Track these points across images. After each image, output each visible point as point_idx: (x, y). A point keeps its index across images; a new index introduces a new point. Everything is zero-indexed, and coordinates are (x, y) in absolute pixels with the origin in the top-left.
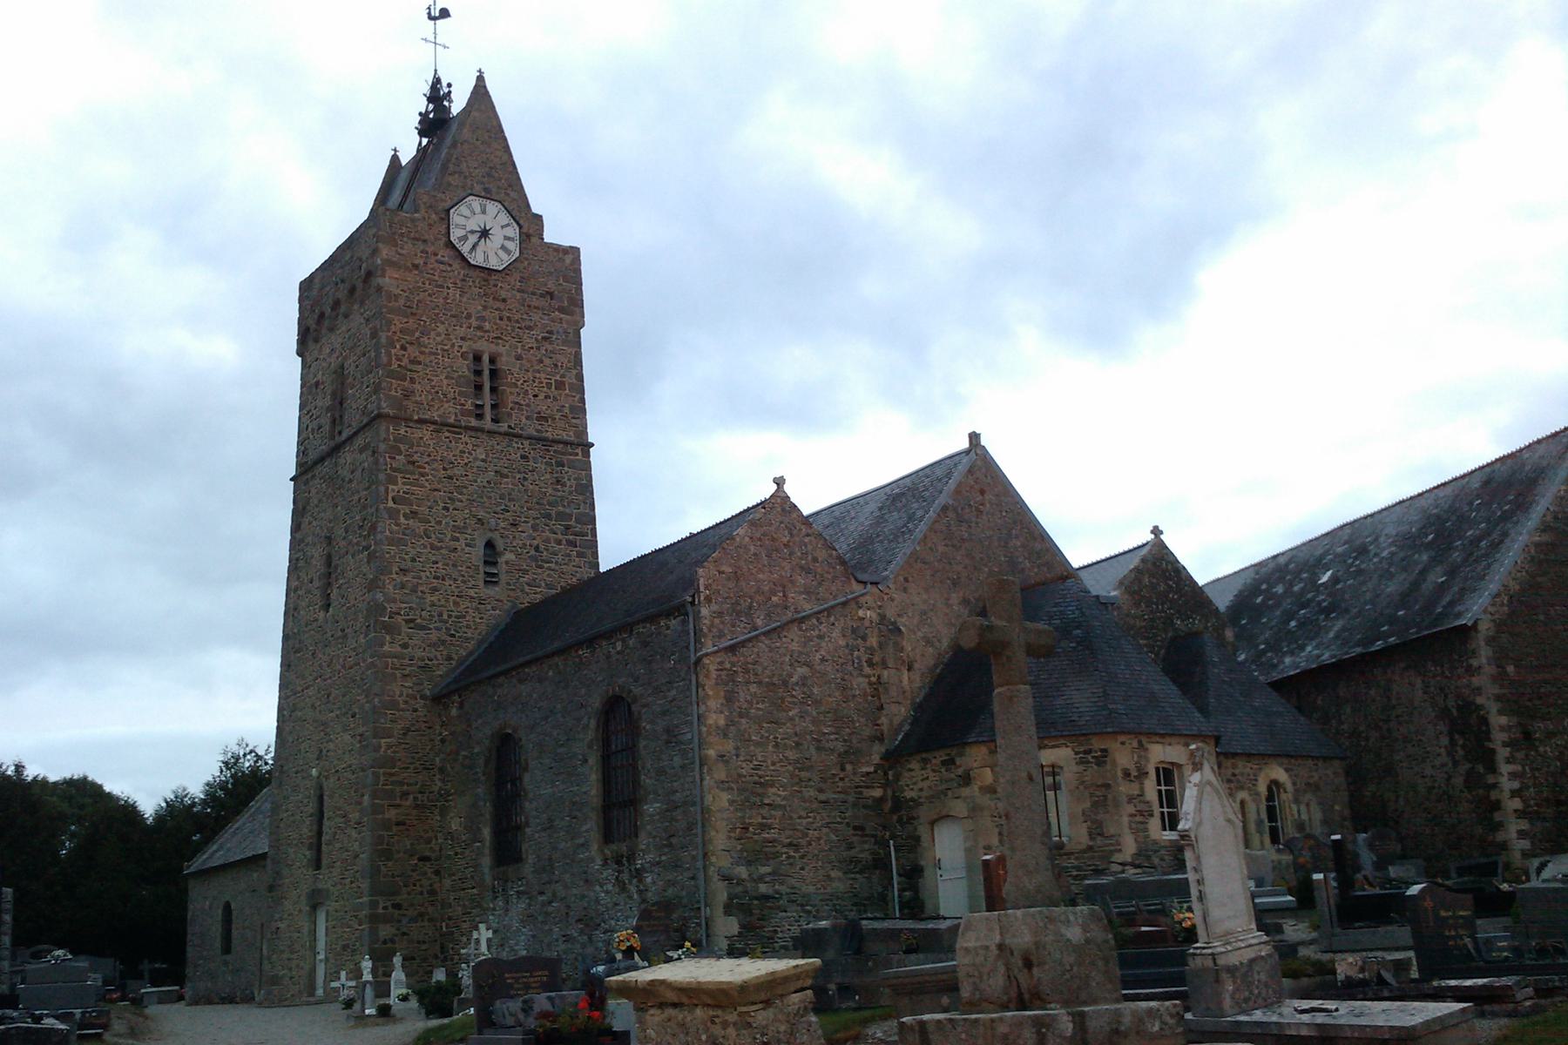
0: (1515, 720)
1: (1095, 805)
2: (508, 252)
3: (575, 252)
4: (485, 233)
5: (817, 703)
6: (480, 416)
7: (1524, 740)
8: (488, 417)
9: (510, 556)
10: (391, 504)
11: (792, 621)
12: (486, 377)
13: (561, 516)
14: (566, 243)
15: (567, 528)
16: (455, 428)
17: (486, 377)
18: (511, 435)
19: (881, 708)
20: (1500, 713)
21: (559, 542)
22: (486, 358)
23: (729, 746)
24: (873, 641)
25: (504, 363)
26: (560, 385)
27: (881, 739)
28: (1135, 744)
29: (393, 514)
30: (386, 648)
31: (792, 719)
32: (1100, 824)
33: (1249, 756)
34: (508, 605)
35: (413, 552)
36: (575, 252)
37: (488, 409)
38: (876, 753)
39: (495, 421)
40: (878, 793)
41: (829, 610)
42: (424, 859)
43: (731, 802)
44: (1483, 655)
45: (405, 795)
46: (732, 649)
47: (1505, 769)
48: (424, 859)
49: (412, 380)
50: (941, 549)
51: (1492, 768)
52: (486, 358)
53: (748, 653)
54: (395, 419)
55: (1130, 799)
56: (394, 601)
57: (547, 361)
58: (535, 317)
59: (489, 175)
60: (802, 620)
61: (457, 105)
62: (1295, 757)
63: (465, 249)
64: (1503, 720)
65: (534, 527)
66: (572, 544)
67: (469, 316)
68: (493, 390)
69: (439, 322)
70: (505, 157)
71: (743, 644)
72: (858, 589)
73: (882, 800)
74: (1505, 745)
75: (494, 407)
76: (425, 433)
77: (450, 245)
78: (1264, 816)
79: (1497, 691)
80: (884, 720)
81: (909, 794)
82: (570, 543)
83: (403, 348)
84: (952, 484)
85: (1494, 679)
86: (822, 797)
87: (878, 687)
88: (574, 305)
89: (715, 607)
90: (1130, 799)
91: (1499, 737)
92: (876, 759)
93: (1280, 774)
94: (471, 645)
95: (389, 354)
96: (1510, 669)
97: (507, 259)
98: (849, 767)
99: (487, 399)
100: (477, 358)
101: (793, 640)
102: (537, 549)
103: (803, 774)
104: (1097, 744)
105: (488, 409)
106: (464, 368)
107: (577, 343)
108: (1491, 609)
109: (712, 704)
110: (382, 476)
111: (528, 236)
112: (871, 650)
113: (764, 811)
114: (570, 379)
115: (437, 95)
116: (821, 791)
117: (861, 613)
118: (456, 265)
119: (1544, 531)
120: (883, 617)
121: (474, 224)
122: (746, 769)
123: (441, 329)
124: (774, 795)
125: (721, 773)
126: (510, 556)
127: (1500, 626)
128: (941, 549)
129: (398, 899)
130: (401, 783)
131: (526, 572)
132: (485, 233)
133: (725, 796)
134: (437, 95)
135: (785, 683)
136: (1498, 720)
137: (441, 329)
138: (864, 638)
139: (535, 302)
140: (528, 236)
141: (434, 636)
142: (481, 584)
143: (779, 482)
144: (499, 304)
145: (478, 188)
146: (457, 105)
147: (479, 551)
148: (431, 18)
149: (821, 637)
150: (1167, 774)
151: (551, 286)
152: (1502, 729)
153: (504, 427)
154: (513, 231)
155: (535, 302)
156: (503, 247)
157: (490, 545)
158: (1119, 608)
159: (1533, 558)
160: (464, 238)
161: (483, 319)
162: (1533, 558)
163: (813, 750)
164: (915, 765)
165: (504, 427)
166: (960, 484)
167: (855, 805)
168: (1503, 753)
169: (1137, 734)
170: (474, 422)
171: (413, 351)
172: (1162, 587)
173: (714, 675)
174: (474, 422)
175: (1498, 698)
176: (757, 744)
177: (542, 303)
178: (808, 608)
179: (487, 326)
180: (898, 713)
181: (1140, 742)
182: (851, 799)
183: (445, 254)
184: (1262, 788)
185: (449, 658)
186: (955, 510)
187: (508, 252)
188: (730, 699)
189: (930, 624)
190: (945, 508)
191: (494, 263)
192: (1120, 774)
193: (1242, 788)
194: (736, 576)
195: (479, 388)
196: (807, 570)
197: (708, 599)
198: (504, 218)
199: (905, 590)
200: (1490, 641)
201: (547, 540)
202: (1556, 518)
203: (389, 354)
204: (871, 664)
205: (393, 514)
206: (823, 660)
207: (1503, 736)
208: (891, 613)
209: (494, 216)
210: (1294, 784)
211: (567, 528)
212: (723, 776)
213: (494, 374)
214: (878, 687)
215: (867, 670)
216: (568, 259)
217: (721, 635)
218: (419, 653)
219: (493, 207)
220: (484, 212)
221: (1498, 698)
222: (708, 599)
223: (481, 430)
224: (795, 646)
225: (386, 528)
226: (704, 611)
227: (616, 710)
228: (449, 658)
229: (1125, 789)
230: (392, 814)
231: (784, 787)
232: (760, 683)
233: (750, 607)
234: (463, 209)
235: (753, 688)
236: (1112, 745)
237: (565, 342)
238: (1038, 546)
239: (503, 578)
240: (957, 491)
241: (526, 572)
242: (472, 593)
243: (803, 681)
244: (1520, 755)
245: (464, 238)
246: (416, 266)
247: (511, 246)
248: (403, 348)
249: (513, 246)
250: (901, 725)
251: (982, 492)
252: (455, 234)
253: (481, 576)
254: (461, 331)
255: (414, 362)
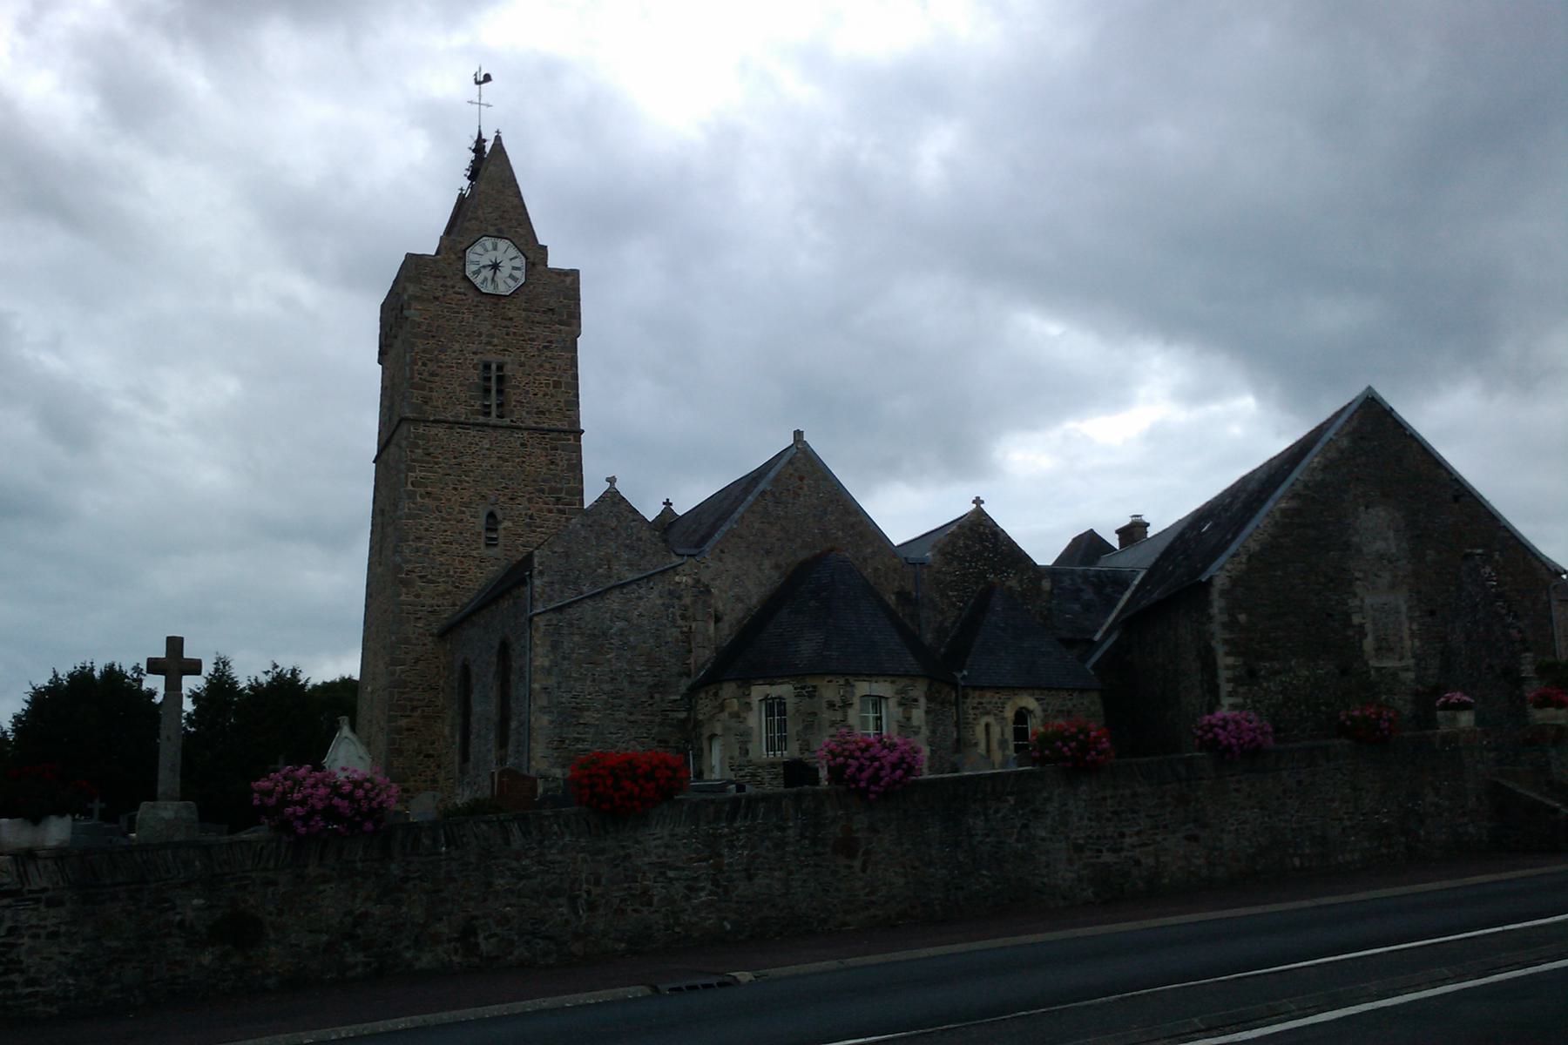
0: (1239, 661)
1: (806, 728)
2: (515, 279)
3: (575, 274)
4: (495, 266)
5: (634, 648)
6: (488, 414)
7: (1248, 677)
8: (494, 414)
9: (507, 524)
10: (410, 487)
11: (614, 587)
12: (494, 381)
13: (553, 490)
14: (567, 267)
15: (558, 499)
16: (464, 425)
17: (494, 381)
18: (512, 428)
19: (690, 651)
20: (1227, 654)
21: (550, 511)
22: (494, 367)
23: (552, 681)
24: (687, 600)
25: (508, 371)
26: (557, 385)
27: (689, 675)
28: (842, 682)
29: (411, 496)
30: (403, 598)
31: (609, 660)
32: (808, 744)
33: (997, 688)
34: (504, 563)
35: (426, 524)
36: (575, 274)
37: (494, 407)
38: (684, 685)
39: (500, 416)
40: (683, 715)
41: (648, 578)
42: (428, 756)
43: (551, 722)
44: (1217, 604)
45: (414, 709)
46: (559, 609)
47: (1226, 701)
48: (428, 756)
49: (431, 390)
50: (756, 525)
51: (1218, 703)
52: (494, 367)
53: (574, 612)
54: (415, 421)
55: (833, 724)
56: (408, 561)
57: (547, 366)
58: (538, 330)
59: (502, 217)
60: (623, 586)
61: (488, 146)
62: (1050, 689)
63: (478, 281)
64: (1230, 660)
65: (530, 500)
66: (561, 512)
67: (480, 335)
68: (500, 392)
69: (478, 325)
70: (516, 201)
71: (569, 605)
72: (676, 560)
73: (686, 720)
74: (1228, 680)
75: (500, 405)
76: (440, 431)
77: (466, 278)
78: (1009, 735)
79: (1227, 636)
80: (692, 660)
81: (700, 717)
82: (561, 512)
83: (424, 364)
84: (772, 474)
85: (1224, 626)
86: (632, 718)
87: (688, 636)
88: (571, 318)
89: (546, 579)
90: (833, 724)
91: (1223, 674)
92: (683, 689)
93: (1029, 702)
94: (471, 595)
95: (412, 370)
96: (1242, 618)
97: (513, 285)
98: (657, 696)
99: (493, 400)
100: (487, 367)
101: (615, 602)
102: (531, 517)
103: (617, 701)
104: (810, 682)
105: (494, 407)
106: (475, 376)
107: (574, 348)
108: (1228, 567)
109: (539, 650)
110: (403, 466)
111: (534, 264)
112: (686, 608)
113: (580, 728)
114: (566, 378)
115: (480, 141)
116: (631, 714)
117: (677, 579)
118: (471, 294)
119: (1292, 498)
120: (698, 581)
121: (486, 260)
122: (566, 698)
123: (457, 346)
124: (588, 717)
125: (543, 701)
126: (507, 524)
127: (1235, 582)
128: (756, 525)
129: (406, 785)
130: (411, 700)
131: (520, 536)
132: (495, 266)
133: (546, 719)
134: (480, 141)
135: (604, 634)
136: (1224, 660)
137: (457, 346)
138: (680, 598)
139: (538, 318)
140: (534, 264)
141: (442, 588)
142: (483, 546)
143: (611, 480)
144: (508, 323)
145: (491, 230)
146: (488, 146)
147: (482, 520)
148: (478, 83)
149: (640, 598)
150: (877, 701)
151: (553, 304)
152: (1228, 667)
153: (507, 421)
154: (520, 262)
155: (538, 318)
156: (511, 276)
157: (491, 515)
158: (929, 566)
159: (1276, 523)
160: (477, 272)
161: (492, 336)
162: (1276, 523)
163: (626, 684)
164: (703, 695)
165: (507, 421)
166: (779, 474)
167: (661, 724)
168: (1226, 687)
169: (844, 674)
170: (481, 419)
171: (432, 366)
172: (978, 547)
173: (542, 629)
174: (481, 419)
175: (1226, 642)
176: (576, 680)
177: (545, 318)
178: (630, 576)
179: (495, 341)
180: (703, 655)
181: (847, 682)
182: (657, 720)
183: (461, 287)
184: (1009, 713)
185: (454, 605)
186: (773, 494)
187: (515, 279)
188: (555, 647)
189: (738, 582)
190: (763, 493)
191: (503, 289)
192: (825, 705)
193: (988, 713)
194: (567, 555)
195: (487, 391)
196: (630, 548)
197: (541, 573)
198: (513, 252)
199: (720, 560)
200: (1223, 593)
201: (541, 510)
202: (1306, 486)
203: (412, 370)
204: (683, 617)
205: (411, 496)
206: (640, 615)
207: (1229, 674)
208: (705, 579)
209: (505, 253)
210: (1044, 710)
211: (558, 499)
212: (545, 703)
213: (501, 379)
214: (688, 636)
215: (680, 622)
216: (568, 280)
217: (551, 599)
218: (431, 602)
219: (503, 244)
220: (495, 248)
221: (1226, 642)
222: (541, 573)
223: (487, 425)
224: (615, 606)
225: (406, 506)
226: (537, 582)
227: (504, 650)
228: (454, 605)
229: (827, 715)
230: (403, 722)
231: (598, 711)
232: (582, 634)
233: (578, 577)
234: (478, 248)
235: (576, 638)
236: (821, 683)
237: (563, 349)
238: (853, 519)
239: (501, 541)
240: (776, 480)
241: (520, 536)
242: (474, 553)
243: (621, 632)
244: (1241, 690)
245: (477, 272)
246: (436, 298)
247: (517, 274)
248: (424, 364)
249: (520, 275)
250: (703, 665)
251: (801, 479)
252: (470, 269)
253: (483, 540)
254: (474, 347)
255: (433, 374)
